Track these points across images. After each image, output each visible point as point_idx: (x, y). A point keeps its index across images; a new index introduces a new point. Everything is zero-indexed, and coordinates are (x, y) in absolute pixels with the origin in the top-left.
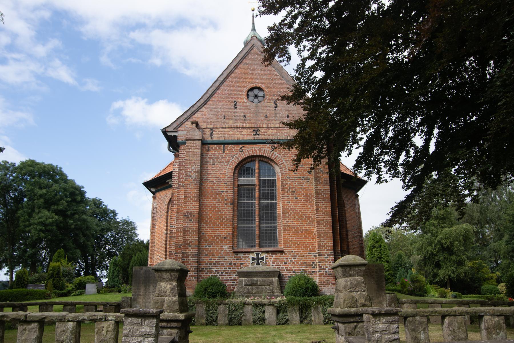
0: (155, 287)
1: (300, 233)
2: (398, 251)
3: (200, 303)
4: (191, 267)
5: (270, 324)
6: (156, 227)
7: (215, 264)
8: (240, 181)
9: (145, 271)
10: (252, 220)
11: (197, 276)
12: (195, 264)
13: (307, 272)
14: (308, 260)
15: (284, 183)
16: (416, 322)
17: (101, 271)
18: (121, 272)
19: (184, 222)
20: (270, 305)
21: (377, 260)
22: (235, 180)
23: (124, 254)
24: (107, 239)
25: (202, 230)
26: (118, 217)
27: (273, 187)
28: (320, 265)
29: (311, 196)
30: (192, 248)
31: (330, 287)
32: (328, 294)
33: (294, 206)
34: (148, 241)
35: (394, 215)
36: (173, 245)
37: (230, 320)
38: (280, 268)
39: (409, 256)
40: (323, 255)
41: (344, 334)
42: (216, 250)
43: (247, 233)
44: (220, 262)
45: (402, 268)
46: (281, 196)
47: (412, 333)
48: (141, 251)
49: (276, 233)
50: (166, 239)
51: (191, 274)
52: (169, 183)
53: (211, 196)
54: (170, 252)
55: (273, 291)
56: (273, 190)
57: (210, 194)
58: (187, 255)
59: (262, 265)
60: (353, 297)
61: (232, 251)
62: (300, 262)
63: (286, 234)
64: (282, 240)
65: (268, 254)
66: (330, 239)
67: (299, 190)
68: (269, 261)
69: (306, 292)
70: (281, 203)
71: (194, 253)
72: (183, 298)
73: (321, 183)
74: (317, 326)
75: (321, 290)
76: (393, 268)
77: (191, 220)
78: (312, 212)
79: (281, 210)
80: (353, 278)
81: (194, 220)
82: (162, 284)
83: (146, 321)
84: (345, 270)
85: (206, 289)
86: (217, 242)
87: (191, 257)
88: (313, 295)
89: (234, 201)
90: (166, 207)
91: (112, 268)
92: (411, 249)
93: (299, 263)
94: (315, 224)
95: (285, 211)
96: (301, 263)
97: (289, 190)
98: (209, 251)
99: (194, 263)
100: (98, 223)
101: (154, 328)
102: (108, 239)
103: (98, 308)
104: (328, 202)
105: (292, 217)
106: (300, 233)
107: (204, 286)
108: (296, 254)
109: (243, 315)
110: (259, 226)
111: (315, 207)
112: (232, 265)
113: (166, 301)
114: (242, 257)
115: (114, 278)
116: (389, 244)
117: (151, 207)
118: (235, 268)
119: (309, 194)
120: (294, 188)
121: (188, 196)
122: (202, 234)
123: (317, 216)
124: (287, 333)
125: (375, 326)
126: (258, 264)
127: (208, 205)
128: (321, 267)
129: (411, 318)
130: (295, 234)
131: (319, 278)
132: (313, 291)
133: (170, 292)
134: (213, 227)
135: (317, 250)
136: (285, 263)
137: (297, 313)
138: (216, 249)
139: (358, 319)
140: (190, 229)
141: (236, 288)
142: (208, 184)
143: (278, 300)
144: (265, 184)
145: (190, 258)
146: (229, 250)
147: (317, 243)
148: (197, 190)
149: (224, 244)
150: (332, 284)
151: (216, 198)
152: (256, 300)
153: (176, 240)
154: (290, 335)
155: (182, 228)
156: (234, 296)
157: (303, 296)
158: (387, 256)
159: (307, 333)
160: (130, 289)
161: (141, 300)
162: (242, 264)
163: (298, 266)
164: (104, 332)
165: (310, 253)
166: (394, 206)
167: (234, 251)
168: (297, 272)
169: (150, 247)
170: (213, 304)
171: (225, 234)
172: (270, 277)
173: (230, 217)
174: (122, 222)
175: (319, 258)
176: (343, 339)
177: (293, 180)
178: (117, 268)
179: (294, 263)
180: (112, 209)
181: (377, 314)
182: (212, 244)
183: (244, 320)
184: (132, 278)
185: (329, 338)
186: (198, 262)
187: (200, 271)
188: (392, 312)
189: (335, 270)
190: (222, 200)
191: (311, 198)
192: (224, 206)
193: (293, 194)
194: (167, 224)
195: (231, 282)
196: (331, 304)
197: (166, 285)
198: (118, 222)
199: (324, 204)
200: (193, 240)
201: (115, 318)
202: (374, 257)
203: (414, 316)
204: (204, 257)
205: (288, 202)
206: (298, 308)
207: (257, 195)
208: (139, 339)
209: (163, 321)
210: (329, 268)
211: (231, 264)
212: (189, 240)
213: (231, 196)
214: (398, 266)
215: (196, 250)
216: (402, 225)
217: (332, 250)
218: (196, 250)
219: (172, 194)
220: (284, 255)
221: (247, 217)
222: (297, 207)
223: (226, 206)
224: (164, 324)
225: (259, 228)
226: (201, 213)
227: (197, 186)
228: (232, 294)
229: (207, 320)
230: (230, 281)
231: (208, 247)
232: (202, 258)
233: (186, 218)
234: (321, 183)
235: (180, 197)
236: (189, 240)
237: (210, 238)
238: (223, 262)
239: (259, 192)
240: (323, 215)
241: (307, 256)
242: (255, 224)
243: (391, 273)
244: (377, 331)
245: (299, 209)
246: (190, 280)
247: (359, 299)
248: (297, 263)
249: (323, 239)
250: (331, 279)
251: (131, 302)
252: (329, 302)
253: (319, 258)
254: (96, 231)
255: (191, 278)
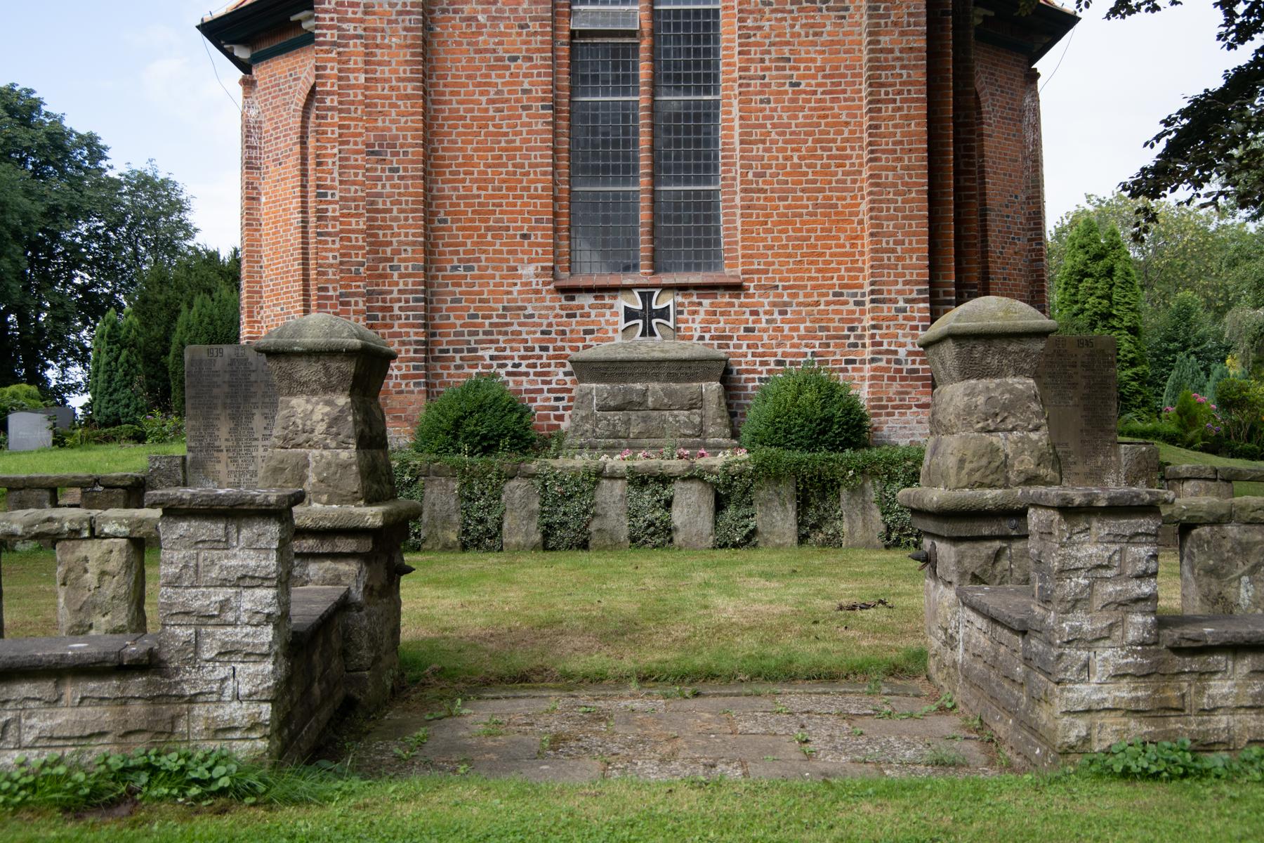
0: (269, 418)
1: (805, 218)
2: (1177, 291)
3: (436, 474)
4: (403, 343)
5: (689, 546)
6: (263, 199)
7: (491, 333)
8: (580, 16)
9: (232, 362)
10: (627, 169)
11: (426, 376)
12: (416, 334)
13: (827, 362)
14: (832, 320)
15: (750, 23)
16: (1224, 542)
17: (63, 368)
18: (140, 366)
19: (368, 178)
20: (691, 478)
21: (1093, 325)
22: (557, 14)
23: (145, 301)
24: (75, 248)
25: (438, 206)
26: (109, 162)
27: (707, 40)
28: (878, 339)
29: (854, 75)
30: (401, 276)
31: (909, 417)
32: (903, 443)
33: (785, 115)
34: (236, 251)
35: (1174, 150)
36: (331, 266)
37: (548, 531)
38: (728, 346)
39: (1220, 313)
40: (890, 300)
41: (955, 579)
42: (491, 282)
43: (606, 219)
44: (507, 324)
45: (1188, 357)
46: (736, 75)
47: (1205, 580)
48: (209, 291)
49: (717, 219)
50: (305, 243)
51: (404, 372)
52: (305, 26)
53: (469, 77)
54: (320, 289)
55: (701, 431)
56: (707, 52)
57: (464, 68)
58: (384, 301)
59: (664, 337)
60: (994, 450)
61: (551, 287)
62: (802, 326)
63: (753, 223)
64: (736, 243)
65: (684, 296)
66: (918, 242)
67: (807, 52)
68: (687, 321)
69: (823, 432)
70: (735, 102)
71: (412, 292)
72: (374, 451)
73: (895, 24)
74: (860, 554)
75: (876, 429)
76: (1154, 355)
77: (397, 170)
78: (854, 140)
79: (737, 130)
80: (997, 381)
81: (405, 170)
82: (295, 401)
83: (245, 533)
84: (971, 352)
85: (457, 424)
86: (495, 252)
87: (401, 309)
88: (848, 444)
89: (557, 96)
90: (296, 122)
91: (104, 355)
92: (1231, 284)
93: (797, 329)
94: (865, 185)
95: (750, 134)
96: (807, 329)
97: (769, 52)
98: (467, 285)
99: (412, 331)
100: (33, 185)
101: (273, 556)
102: (81, 246)
103: (64, 496)
104: (917, 100)
105: (777, 158)
106: (805, 218)
107: (450, 413)
108: (789, 295)
109: (594, 515)
110: (653, 192)
111: (866, 119)
112: (553, 335)
113: (313, 465)
114: (591, 307)
115: (115, 390)
116: (1145, 267)
117: (239, 123)
118: (563, 348)
119: (846, 67)
120: (788, 43)
121: (378, 75)
122: (440, 221)
123: (872, 152)
124: (750, 575)
125: (1067, 550)
126: (648, 331)
127: (458, 110)
128: (881, 344)
129: (1207, 529)
130: (788, 223)
131: (870, 386)
132: (847, 431)
133: (327, 432)
134: (479, 196)
135: (867, 282)
136: (747, 330)
137: (789, 506)
138: (493, 277)
139: (1007, 526)
140: (392, 203)
141: (566, 417)
142: (454, 27)
143: (719, 460)
144: (677, 27)
145: (397, 312)
146: (541, 281)
147: (867, 257)
148: (413, 54)
149: (522, 261)
150: (917, 406)
151: (486, 84)
152: (641, 461)
153: (342, 247)
154: (762, 581)
155: (363, 199)
156: (559, 448)
157: (810, 448)
158: (1132, 310)
159: (820, 575)
160: (178, 430)
161: (222, 467)
162: (591, 332)
163: (796, 340)
164: (91, 578)
165: (841, 294)
166: (1173, 111)
167: (560, 284)
168: (792, 363)
169: (244, 274)
170: (484, 475)
171: (524, 221)
172: (690, 378)
173: (542, 157)
174: (130, 184)
175: (873, 310)
176: (950, 594)
177: (783, 11)
178: (125, 352)
179: (781, 330)
180: (83, 131)
181: (1079, 507)
182: (478, 260)
183: (599, 530)
184: (183, 389)
185: (899, 595)
186: (425, 326)
187: (436, 359)
188: (1136, 502)
189: (930, 351)
190: (510, 92)
191: (854, 83)
192: (520, 117)
193: (784, 69)
194: (304, 186)
195: (548, 399)
196: (913, 478)
197: (310, 407)
198: (112, 180)
199: (900, 109)
200: (407, 244)
201: (129, 525)
202: (1082, 311)
203: (1218, 521)
204: (448, 309)
205: (762, 101)
206: (792, 489)
207: (644, 71)
208: (220, 595)
209: (303, 533)
210: (910, 348)
211: (549, 333)
212: (391, 243)
213: (546, 75)
214: (1172, 346)
215: (419, 284)
216: (1202, 187)
217: (923, 283)
218: (419, 284)
219: (317, 68)
220: (743, 300)
221: (605, 157)
222: (796, 117)
223: (527, 116)
224: (311, 542)
225: (653, 201)
226: (431, 142)
227: (414, 38)
228: (555, 441)
229: (466, 532)
230: (546, 395)
231: (461, 272)
232: (440, 310)
233: (377, 162)
234: (895, 24)
235: (348, 79)
236: (391, 243)
237: (471, 237)
238: (520, 324)
239: (653, 60)
240: (895, 151)
241: (828, 303)
242: (636, 183)
243: (1145, 373)
244: (1077, 569)
245: (805, 125)
246: (401, 392)
247: (1014, 458)
248: (791, 329)
249: (891, 240)
250: (915, 387)
251: (185, 471)
252: (906, 470)
253: (873, 310)
254: (27, 218)
255: (404, 383)
